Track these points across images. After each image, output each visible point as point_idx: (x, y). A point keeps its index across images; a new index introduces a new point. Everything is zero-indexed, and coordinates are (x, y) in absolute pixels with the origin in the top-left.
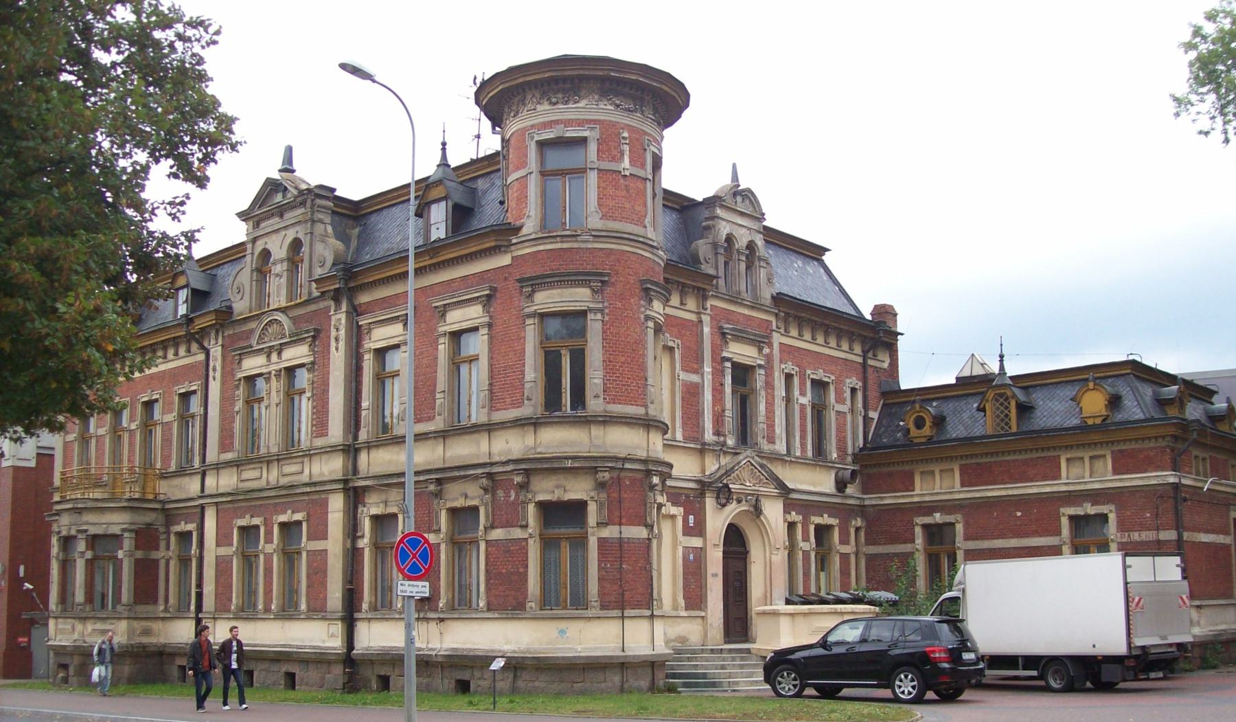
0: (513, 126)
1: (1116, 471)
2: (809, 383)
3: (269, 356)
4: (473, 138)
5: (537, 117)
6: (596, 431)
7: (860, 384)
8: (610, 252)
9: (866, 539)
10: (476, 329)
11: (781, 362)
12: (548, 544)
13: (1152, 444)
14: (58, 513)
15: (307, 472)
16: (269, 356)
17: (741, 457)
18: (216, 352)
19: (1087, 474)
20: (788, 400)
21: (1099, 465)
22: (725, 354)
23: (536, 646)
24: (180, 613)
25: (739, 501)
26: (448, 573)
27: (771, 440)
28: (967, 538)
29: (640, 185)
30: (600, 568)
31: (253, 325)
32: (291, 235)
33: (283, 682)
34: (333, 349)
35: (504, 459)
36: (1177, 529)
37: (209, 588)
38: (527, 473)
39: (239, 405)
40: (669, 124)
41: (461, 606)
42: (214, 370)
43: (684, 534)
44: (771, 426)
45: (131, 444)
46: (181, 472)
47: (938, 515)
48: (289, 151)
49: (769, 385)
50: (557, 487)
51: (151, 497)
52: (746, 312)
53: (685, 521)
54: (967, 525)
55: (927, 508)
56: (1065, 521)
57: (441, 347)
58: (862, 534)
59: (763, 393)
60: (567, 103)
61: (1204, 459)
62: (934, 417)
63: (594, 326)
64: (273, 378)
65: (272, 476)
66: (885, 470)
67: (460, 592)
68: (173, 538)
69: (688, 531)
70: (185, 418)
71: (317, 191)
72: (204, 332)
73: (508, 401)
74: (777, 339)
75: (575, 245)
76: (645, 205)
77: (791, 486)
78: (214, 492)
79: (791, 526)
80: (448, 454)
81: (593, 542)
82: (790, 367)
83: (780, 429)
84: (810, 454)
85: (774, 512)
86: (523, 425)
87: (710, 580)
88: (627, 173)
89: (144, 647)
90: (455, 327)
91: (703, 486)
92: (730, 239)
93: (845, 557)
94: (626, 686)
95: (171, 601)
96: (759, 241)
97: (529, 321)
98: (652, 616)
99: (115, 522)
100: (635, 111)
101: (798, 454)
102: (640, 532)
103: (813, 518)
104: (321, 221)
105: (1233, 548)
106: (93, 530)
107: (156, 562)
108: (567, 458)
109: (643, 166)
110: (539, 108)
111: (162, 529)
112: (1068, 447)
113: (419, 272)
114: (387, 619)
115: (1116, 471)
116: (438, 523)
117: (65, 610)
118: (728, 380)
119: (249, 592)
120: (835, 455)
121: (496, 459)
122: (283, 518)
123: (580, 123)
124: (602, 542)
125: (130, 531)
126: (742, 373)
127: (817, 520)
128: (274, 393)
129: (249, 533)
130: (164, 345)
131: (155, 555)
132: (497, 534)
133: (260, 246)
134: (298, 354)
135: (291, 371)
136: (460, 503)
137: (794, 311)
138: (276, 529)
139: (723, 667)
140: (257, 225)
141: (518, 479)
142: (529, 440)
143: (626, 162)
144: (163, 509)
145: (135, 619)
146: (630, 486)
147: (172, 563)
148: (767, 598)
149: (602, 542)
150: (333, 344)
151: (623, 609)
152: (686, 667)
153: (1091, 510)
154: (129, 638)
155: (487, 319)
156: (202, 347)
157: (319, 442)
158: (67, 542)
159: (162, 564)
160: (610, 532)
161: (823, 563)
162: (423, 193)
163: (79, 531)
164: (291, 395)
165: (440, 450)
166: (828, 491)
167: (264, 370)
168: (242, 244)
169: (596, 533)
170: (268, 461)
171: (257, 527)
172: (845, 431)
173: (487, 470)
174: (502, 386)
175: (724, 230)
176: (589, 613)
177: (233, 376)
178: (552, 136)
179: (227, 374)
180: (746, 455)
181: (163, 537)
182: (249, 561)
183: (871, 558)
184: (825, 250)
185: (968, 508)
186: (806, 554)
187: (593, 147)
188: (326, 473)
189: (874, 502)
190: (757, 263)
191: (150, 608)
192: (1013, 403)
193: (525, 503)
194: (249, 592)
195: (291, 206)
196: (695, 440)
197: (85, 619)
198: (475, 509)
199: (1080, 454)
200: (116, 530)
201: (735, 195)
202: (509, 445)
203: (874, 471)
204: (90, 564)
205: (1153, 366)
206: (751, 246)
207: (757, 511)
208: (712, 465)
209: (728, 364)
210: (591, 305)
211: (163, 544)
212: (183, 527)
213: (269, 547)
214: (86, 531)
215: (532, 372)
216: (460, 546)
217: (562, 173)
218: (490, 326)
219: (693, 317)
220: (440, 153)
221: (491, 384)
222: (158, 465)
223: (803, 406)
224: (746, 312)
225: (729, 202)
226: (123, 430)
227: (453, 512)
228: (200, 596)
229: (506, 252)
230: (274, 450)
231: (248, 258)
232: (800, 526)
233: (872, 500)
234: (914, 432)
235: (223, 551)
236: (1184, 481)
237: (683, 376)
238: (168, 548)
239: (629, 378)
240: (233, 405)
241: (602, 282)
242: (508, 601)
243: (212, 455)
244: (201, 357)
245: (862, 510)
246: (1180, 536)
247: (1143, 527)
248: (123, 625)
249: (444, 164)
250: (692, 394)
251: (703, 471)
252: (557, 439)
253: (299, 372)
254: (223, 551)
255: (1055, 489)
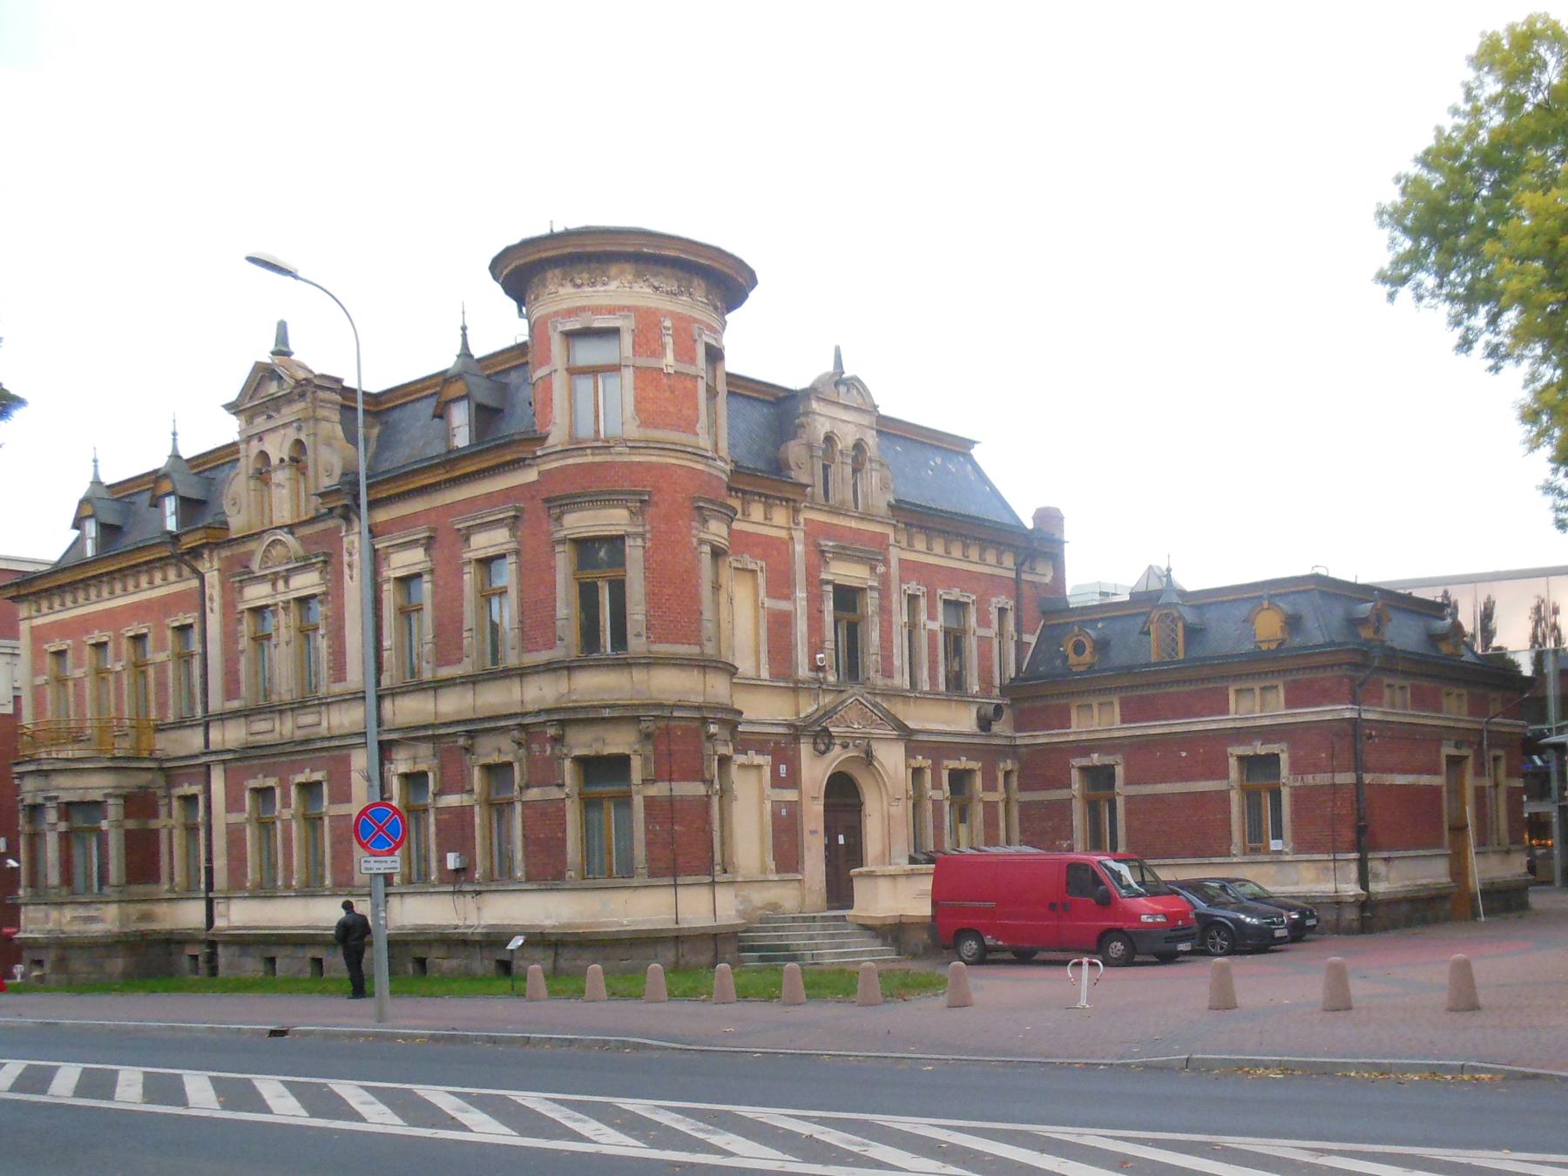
0: (539, 311)
1: (1290, 703)
2: (940, 606)
3: (274, 585)
4: (500, 325)
5: (565, 297)
6: (639, 675)
7: (1012, 603)
8: (650, 467)
9: (1019, 785)
10: (503, 556)
11: (902, 580)
12: (590, 804)
13: (1329, 673)
14: (22, 775)
15: (325, 724)
16: (274, 585)
17: (844, 696)
18: (212, 578)
19: (1258, 708)
20: (912, 627)
21: (1270, 696)
22: (824, 576)
23: (578, 920)
24: (188, 894)
25: (845, 746)
26: (484, 838)
27: (888, 673)
28: (1129, 781)
29: (689, 384)
30: (647, 831)
31: (252, 545)
32: (291, 434)
33: (309, 970)
34: (347, 577)
35: (536, 708)
36: (1356, 770)
37: (220, 863)
38: (562, 723)
39: (244, 643)
40: (729, 310)
41: (500, 879)
42: (211, 599)
43: (773, 786)
44: (887, 657)
45: (119, 689)
46: (181, 724)
47: (1095, 756)
48: (282, 329)
49: (885, 610)
50: (596, 740)
51: (145, 754)
52: (854, 524)
53: (775, 771)
54: (1127, 769)
55: (1084, 748)
56: (1233, 762)
57: (466, 577)
58: (1014, 779)
59: (876, 619)
60: (593, 284)
61: (1402, 688)
62: (1095, 642)
63: (634, 552)
64: (281, 612)
65: (286, 728)
66: (1040, 704)
67: (501, 861)
68: (176, 804)
69: (777, 782)
70: (184, 658)
71: (316, 382)
72: (195, 552)
73: (540, 641)
74: (895, 555)
75: (609, 458)
76: (696, 408)
77: (912, 725)
78: (220, 748)
79: (917, 772)
80: (479, 703)
81: (638, 802)
82: (912, 587)
83: (900, 659)
84: (942, 687)
85: (892, 758)
86: (555, 670)
87: (807, 836)
88: (671, 371)
89: (143, 934)
90: (481, 554)
91: (796, 731)
92: (829, 439)
93: (990, 807)
94: (682, 962)
95: (177, 879)
96: (871, 440)
97: (559, 548)
98: (713, 884)
99: (96, 786)
100: (681, 293)
101: (926, 688)
102: (695, 789)
103: (946, 762)
104: (327, 420)
105: (1444, 789)
106: (66, 797)
107: (156, 832)
108: (605, 707)
109: (693, 361)
110: (562, 291)
111: (161, 793)
112: (1237, 677)
113: (373, 504)
114: (421, 893)
115: (1290, 703)
116: (471, 783)
117: (36, 895)
118: (829, 606)
119: (268, 864)
120: (976, 688)
121: (530, 708)
122: (301, 778)
123: (612, 310)
124: (650, 802)
125: (117, 796)
126: (847, 597)
127: (953, 764)
128: (283, 630)
129: (264, 794)
130: (150, 565)
131: (153, 824)
132: (534, 794)
133: (255, 447)
134: (307, 582)
135: (303, 601)
136: (495, 758)
137: (915, 518)
138: (293, 792)
139: (811, 938)
140: (250, 421)
141: (551, 731)
142: (563, 686)
143: (669, 358)
144: (161, 769)
145: (129, 902)
146: (685, 739)
147: (176, 833)
148: (886, 856)
149: (650, 802)
150: (346, 570)
151: (675, 876)
152: (769, 938)
153: (1261, 749)
154: (122, 925)
155: (513, 546)
156: (196, 571)
157: (337, 688)
158: (35, 810)
159: (164, 834)
160: (659, 790)
161: (962, 814)
162: (435, 392)
163: (47, 799)
164: (306, 632)
165: (469, 696)
166: (966, 730)
167: (270, 601)
168: (234, 444)
169: (643, 789)
170: (279, 710)
171: (271, 789)
172: (990, 659)
173: (518, 721)
174: (536, 621)
175: (821, 427)
176: (635, 882)
177: (235, 607)
178: (578, 326)
179: (229, 606)
180: (854, 692)
181: (163, 802)
182: (265, 826)
183: (1025, 807)
184: (972, 443)
185: (1137, 748)
186: (937, 805)
187: (627, 340)
188: (346, 723)
189: (1027, 742)
190: (868, 465)
191: (151, 888)
192: (1180, 625)
193: (562, 758)
194: (268, 864)
195: (288, 399)
196: (786, 678)
197: (62, 904)
198: (510, 765)
199: (1274, 683)
200: (96, 796)
201: (837, 384)
202: (541, 692)
203: (1026, 705)
204: (65, 838)
205: (1352, 580)
206: (859, 446)
207: (868, 758)
208: (808, 708)
209: (830, 588)
210: (629, 529)
211: (163, 811)
212: (187, 789)
213: (288, 811)
214: (56, 798)
215: (566, 607)
216: (499, 808)
217: (593, 371)
218: (517, 552)
219: (783, 534)
220: (460, 340)
221: (521, 622)
222: (153, 715)
223: (932, 635)
224: (854, 524)
225: (830, 393)
226: (108, 671)
227: (488, 769)
228: (210, 871)
229: (530, 465)
230: (287, 697)
231: (243, 461)
232: (928, 773)
233: (1023, 739)
234: (1073, 659)
235: (236, 818)
236: (1364, 716)
237: (768, 603)
238: (170, 815)
239: (680, 612)
240: (236, 642)
241: (642, 501)
242: (547, 871)
243: (216, 704)
244: (195, 583)
245: (1012, 750)
246: (1359, 779)
247: (1317, 768)
248: (112, 911)
249: (465, 353)
250: (780, 626)
251: (797, 714)
252: (593, 685)
253: (314, 604)
254: (236, 818)
255: (1222, 725)
